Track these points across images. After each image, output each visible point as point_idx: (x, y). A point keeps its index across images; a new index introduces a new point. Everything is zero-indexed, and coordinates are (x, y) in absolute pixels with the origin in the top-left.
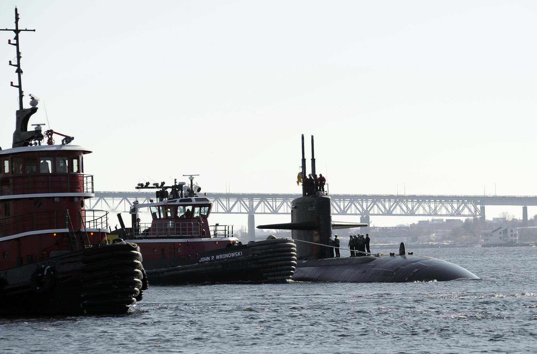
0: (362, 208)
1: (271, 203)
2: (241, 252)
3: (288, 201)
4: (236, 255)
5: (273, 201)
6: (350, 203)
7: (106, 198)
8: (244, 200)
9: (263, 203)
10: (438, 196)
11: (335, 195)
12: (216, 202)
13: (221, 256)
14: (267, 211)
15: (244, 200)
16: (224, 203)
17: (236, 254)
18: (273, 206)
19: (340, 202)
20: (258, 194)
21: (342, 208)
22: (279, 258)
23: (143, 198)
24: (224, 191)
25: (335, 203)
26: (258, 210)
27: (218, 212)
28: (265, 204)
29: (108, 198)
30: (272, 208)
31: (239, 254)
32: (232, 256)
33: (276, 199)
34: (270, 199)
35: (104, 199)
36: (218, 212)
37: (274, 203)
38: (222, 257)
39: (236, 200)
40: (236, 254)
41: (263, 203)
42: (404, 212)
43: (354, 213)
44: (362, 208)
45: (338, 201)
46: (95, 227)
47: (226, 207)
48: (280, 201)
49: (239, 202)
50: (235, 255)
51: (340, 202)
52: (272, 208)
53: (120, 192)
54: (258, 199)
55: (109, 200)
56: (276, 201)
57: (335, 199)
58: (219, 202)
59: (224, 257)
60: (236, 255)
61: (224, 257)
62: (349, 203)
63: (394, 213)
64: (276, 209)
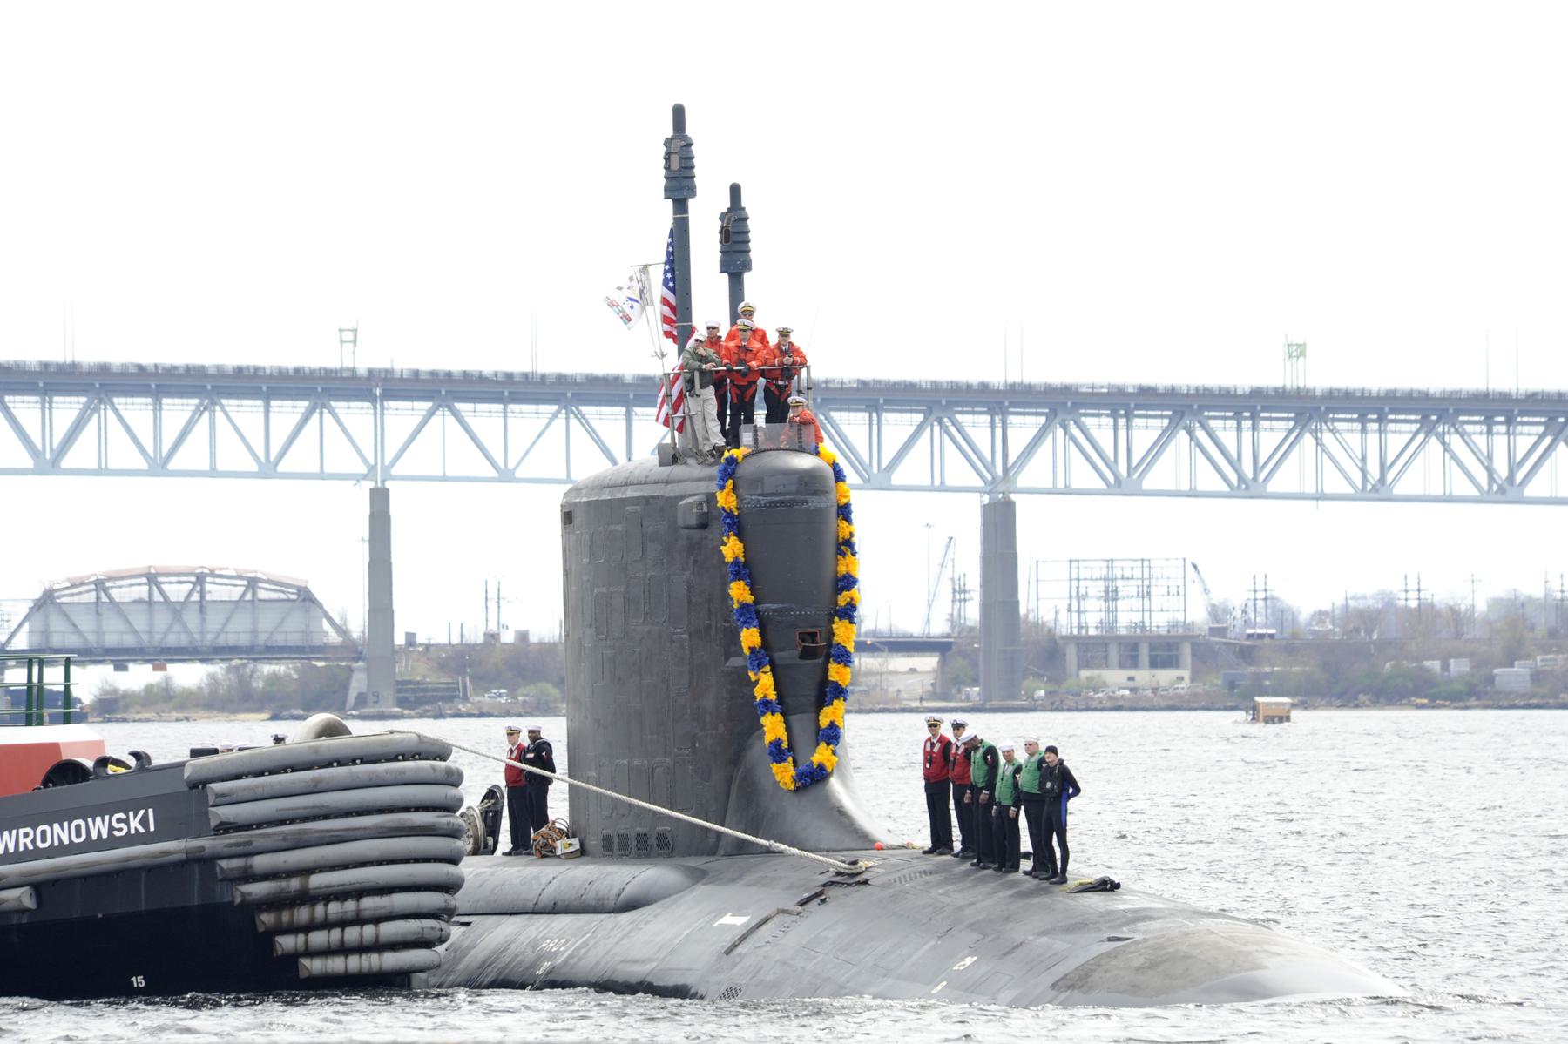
0: (1490, 471)
1: (1228, 437)
2: (146, 815)
3: (1324, 427)
4: (120, 830)
5: (1239, 428)
6: (1548, 440)
7: (122, 400)
8: (1213, 423)
9: (1183, 436)
10: (1251, 392)
11: (863, 383)
12: (937, 428)
13: (26, 835)
14: (1209, 480)
15: (1213, 423)
16: (1228, 437)
17: (119, 821)
18: (1239, 455)
19: (1489, 432)
20: (957, 384)
21: (1502, 470)
22: (389, 930)
23: (906, 411)
24: (1469, 380)
25: (1462, 437)
26: (1035, 473)
27: (942, 483)
28: (1073, 439)
29: (480, 407)
30: (1235, 464)
31: (135, 824)
32: (94, 837)
33: (1254, 418)
34: (1225, 418)
35: (457, 415)
36: (942, 483)
37: (1247, 436)
38: (34, 841)
39: (1042, 420)
40: (119, 821)
41: (1183, 436)
42: (1477, 485)
43: (1441, 493)
44: (1490, 471)
45: (1478, 428)
46: (1083, 632)
47: (989, 458)
48: (1276, 424)
49: (1060, 432)
50: (111, 828)
51: (1489, 432)
52: (1235, 464)
53: (864, 384)
54: (1222, 414)
55: (484, 417)
56: (1254, 428)
57: (1206, 414)
58: (953, 429)
59: (44, 840)
60: (120, 830)
61: (44, 840)
62: (1541, 437)
63: (1529, 491)
64: (1256, 469)
